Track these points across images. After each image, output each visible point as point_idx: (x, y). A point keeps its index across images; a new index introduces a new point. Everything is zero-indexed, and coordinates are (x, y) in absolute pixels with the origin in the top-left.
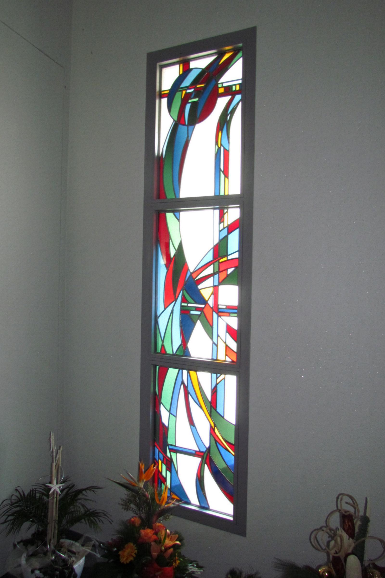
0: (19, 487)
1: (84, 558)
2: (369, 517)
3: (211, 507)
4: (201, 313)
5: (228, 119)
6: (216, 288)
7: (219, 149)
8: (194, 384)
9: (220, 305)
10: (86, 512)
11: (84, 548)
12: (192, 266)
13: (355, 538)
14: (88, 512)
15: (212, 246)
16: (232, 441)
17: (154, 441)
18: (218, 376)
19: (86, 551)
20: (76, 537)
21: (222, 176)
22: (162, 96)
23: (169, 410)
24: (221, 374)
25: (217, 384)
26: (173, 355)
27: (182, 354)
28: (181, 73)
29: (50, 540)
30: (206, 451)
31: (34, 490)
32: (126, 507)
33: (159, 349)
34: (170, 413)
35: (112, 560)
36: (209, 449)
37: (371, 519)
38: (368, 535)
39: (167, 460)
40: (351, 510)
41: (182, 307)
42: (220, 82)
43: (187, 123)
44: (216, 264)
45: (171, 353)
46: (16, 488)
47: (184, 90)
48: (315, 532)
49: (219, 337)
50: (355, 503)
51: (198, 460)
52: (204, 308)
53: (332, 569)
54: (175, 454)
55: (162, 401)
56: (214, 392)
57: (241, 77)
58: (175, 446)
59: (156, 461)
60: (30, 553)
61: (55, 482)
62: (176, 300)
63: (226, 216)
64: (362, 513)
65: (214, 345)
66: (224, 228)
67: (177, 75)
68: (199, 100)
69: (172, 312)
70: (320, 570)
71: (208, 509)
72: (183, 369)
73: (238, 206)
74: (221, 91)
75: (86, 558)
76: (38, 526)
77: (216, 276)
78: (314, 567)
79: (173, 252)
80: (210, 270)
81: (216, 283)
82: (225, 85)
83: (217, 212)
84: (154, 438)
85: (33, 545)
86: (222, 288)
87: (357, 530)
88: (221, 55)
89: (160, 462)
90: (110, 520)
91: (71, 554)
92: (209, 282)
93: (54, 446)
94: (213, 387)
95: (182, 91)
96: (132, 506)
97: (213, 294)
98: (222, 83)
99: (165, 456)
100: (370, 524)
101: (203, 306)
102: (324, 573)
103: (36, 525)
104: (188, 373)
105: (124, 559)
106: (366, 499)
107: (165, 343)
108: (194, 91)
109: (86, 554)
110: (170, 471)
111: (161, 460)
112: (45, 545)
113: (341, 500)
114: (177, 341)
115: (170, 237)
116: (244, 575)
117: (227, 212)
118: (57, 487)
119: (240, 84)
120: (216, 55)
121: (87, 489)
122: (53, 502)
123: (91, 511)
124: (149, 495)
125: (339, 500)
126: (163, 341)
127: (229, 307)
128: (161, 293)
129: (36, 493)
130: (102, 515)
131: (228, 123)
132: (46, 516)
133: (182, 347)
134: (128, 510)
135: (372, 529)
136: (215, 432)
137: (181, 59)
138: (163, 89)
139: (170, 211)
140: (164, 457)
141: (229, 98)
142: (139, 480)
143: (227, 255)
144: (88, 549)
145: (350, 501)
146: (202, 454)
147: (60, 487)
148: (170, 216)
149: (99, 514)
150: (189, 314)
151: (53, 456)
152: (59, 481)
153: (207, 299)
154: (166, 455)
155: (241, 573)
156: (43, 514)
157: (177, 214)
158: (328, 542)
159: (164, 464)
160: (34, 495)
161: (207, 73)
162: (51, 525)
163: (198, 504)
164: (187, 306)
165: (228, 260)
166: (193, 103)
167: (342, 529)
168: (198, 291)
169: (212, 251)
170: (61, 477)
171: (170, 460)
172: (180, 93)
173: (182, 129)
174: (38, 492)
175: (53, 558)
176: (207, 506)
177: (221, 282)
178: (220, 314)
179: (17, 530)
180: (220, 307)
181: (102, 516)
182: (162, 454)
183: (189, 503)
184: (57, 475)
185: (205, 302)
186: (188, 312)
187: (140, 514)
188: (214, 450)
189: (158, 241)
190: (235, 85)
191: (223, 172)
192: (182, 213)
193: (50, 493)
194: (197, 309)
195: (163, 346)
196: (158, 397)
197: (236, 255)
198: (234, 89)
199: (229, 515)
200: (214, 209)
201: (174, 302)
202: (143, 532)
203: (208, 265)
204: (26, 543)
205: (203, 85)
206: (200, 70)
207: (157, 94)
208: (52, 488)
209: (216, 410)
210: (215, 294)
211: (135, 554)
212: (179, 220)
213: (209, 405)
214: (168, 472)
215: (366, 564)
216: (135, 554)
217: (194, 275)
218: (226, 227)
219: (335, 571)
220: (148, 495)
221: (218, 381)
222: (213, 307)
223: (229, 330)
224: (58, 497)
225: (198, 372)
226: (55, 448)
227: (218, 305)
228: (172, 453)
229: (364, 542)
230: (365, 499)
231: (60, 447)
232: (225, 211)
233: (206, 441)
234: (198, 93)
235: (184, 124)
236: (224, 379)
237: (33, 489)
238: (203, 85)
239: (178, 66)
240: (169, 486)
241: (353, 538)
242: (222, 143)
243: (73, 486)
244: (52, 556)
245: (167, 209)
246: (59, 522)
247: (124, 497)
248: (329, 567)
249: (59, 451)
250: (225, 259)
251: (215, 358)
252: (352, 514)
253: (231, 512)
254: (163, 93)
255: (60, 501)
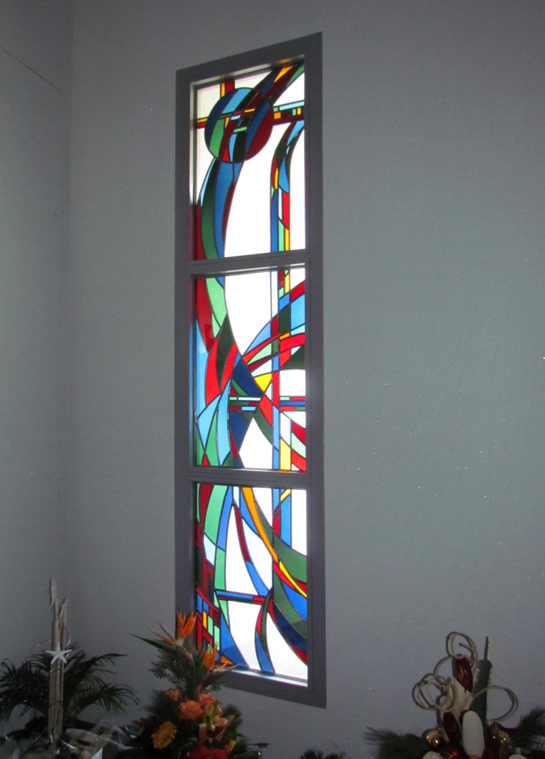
0: (6, 659)
1: (101, 751)
2: (491, 661)
3: (277, 672)
4: (256, 409)
5: (287, 153)
6: (275, 376)
7: (276, 192)
8: (250, 508)
9: (282, 396)
10: (102, 689)
11: (102, 737)
12: (243, 347)
13: (473, 689)
14: (105, 689)
15: (268, 319)
16: (304, 579)
17: (196, 586)
18: (282, 492)
19: (104, 741)
20: (88, 726)
21: (281, 226)
22: (197, 125)
23: (215, 542)
24: (286, 489)
25: (280, 503)
26: (220, 467)
27: (232, 465)
28: (223, 94)
29: (53, 730)
30: (268, 594)
31: (28, 663)
32: (159, 672)
33: (200, 461)
34: (217, 547)
35: (141, 748)
36: (271, 592)
37: (493, 664)
38: (490, 685)
39: (215, 612)
40: (467, 654)
41: (230, 402)
42: (275, 105)
43: (232, 160)
44: (276, 342)
45: (217, 465)
46: (4, 661)
47: (228, 117)
48: (417, 689)
49: (281, 440)
50: (473, 646)
51: (257, 608)
52: (259, 402)
53: (444, 734)
54: (225, 602)
55: (206, 530)
56: (277, 513)
57: (302, 97)
58: (225, 591)
59: (199, 613)
60: (25, 749)
61: (58, 647)
62: (222, 393)
63: (287, 279)
64: (481, 657)
65: (275, 450)
66: (285, 294)
67: (218, 98)
68: (248, 129)
69: (217, 410)
70: (428, 737)
71: (273, 674)
72: (233, 485)
73: (303, 264)
74: (277, 116)
75: (104, 751)
76: (34, 711)
77: (276, 359)
78: (419, 735)
79: (216, 330)
80: (267, 351)
81: (276, 368)
82: (282, 108)
83: (275, 274)
84: (195, 583)
85: (27, 737)
86: (284, 375)
87: (475, 680)
88: (275, 70)
89: (205, 615)
90: (136, 700)
91: (82, 746)
92: (267, 367)
93: (56, 600)
94: (275, 508)
95: (225, 118)
96: (168, 672)
97: (272, 383)
98: (278, 107)
99: (211, 606)
100: (493, 670)
101: (258, 399)
102: (433, 741)
103: (32, 709)
104: (241, 490)
105: (159, 743)
106: (487, 638)
107: (208, 453)
108: (241, 117)
109: (104, 745)
110: (219, 626)
111: (206, 612)
112: (46, 735)
113: (453, 641)
114: (224, 449)
115: (212, 310)
116: (324, 756)
117: (289, 273)
118: (61, 654)
119: (302, 108)
120: (271, 70)
121: (103, 657)
122: (56, 676)
123: (109, 687)
124: (191, 656)
125: (450, 641)
126: (205, 449)
127: (294, 399)
128: (200, 394)
129: (30, 667)
130: (125, 692)
131: (288, 158)
132: (46, 696)
133: (232, 456)
134: (163, 677)
135: (494, 677)
136: (279, 568)
137: (223, 76)
138: (199, 116)
139: (211, 276)
140: (210, 607)
141: (286, 126)
142: (176, 637)
143: (290, 330)
144: (107, 737)
145: (466, 642)
146: (263, 600)
147: (65, 654)
148: (211, 283)
149: (121, 691)
150: (239, 411)
151: (54, 611)
152: (64, 645)
153: (263, 389)
154: (213, 604)
155: (320, 755)
156: (42, 694)
157: (220, 279)
158: (438, 699)
159: (211, 617)
160: (28, 669)
161: (257, 94)
162: (53, 708)
163: (259, 668)
164: (238, 401)
165: (291, 337)
166: (240, 134)
167: (455, 679)
168: (252, 379)
169: (269, 325)
170: (67, 642)
171: (218, 611)
172: (222, 121)
173: (226, 168)
174: (34, 665)
175: (58, 751)
176: (271, 671)
177: (284, 366)
178: (282, 408)
179: (5, 718)
180: (282, 399)
181: (124, 694)
182: (207, 603)
183: (246, 668)
184: (62, 639)
185: (260, 393)
186: (239, 408)
187: (179, 683)
188: (279, 592)
189: (196, 316)
190: (296, 108)
191: (282, 221)
192: (227, 278)
193: (52, 662)
194: (252, 404)
195: (205, 457)
196: (200, 526)
197: (302, 330)
198: (294, 113)
199: (302, 681)
200: (271, 270)
201: (219, 396)
202: (184, 707)
203: (265, 343)
204: (18, 735)
205: (253, 110)
206: (250, 90)
207: (192, 123)
208: (54, 656)
209: (280, 538)
210: (275, 382)
211: (174, 734)
212: (223, 287)
213: (271, 531)
214: (216, 627)
215: (490, 723)
216: (174, 734)
217: (246, 359)
218: (287, 294)
219: (448, 735)
220: (190, 656)
221: (283, 497)
222: (272, 399)
223: (295, 429)
224: (63, 669)
225: (254, 489)
226: (57, 602)
227: (280, 397)
228: (221, 601)
229: (485, 694)
230: (485, 639)
231: (64, 600)
232: (286, 272)
233: (268, 582)
234: (246, 120)
235: (228, 161)
236: (290, 495)
237: (27, 663)
238: (253, 110)
239: (218, 86)
240: (218, 648)
241: (470, 691)
242: (280, 184)
243: (83, 655)
244: (56, 750)
245: (208, 273)
246: (65, 704)
247: (157, 660)
248: (440, 732)
249: (63, 606)
250: (287, 335)
251: (277, 468)
252: (468, 660)
253: (305, 677)
254: (199, 121)
255: (66, 675)
